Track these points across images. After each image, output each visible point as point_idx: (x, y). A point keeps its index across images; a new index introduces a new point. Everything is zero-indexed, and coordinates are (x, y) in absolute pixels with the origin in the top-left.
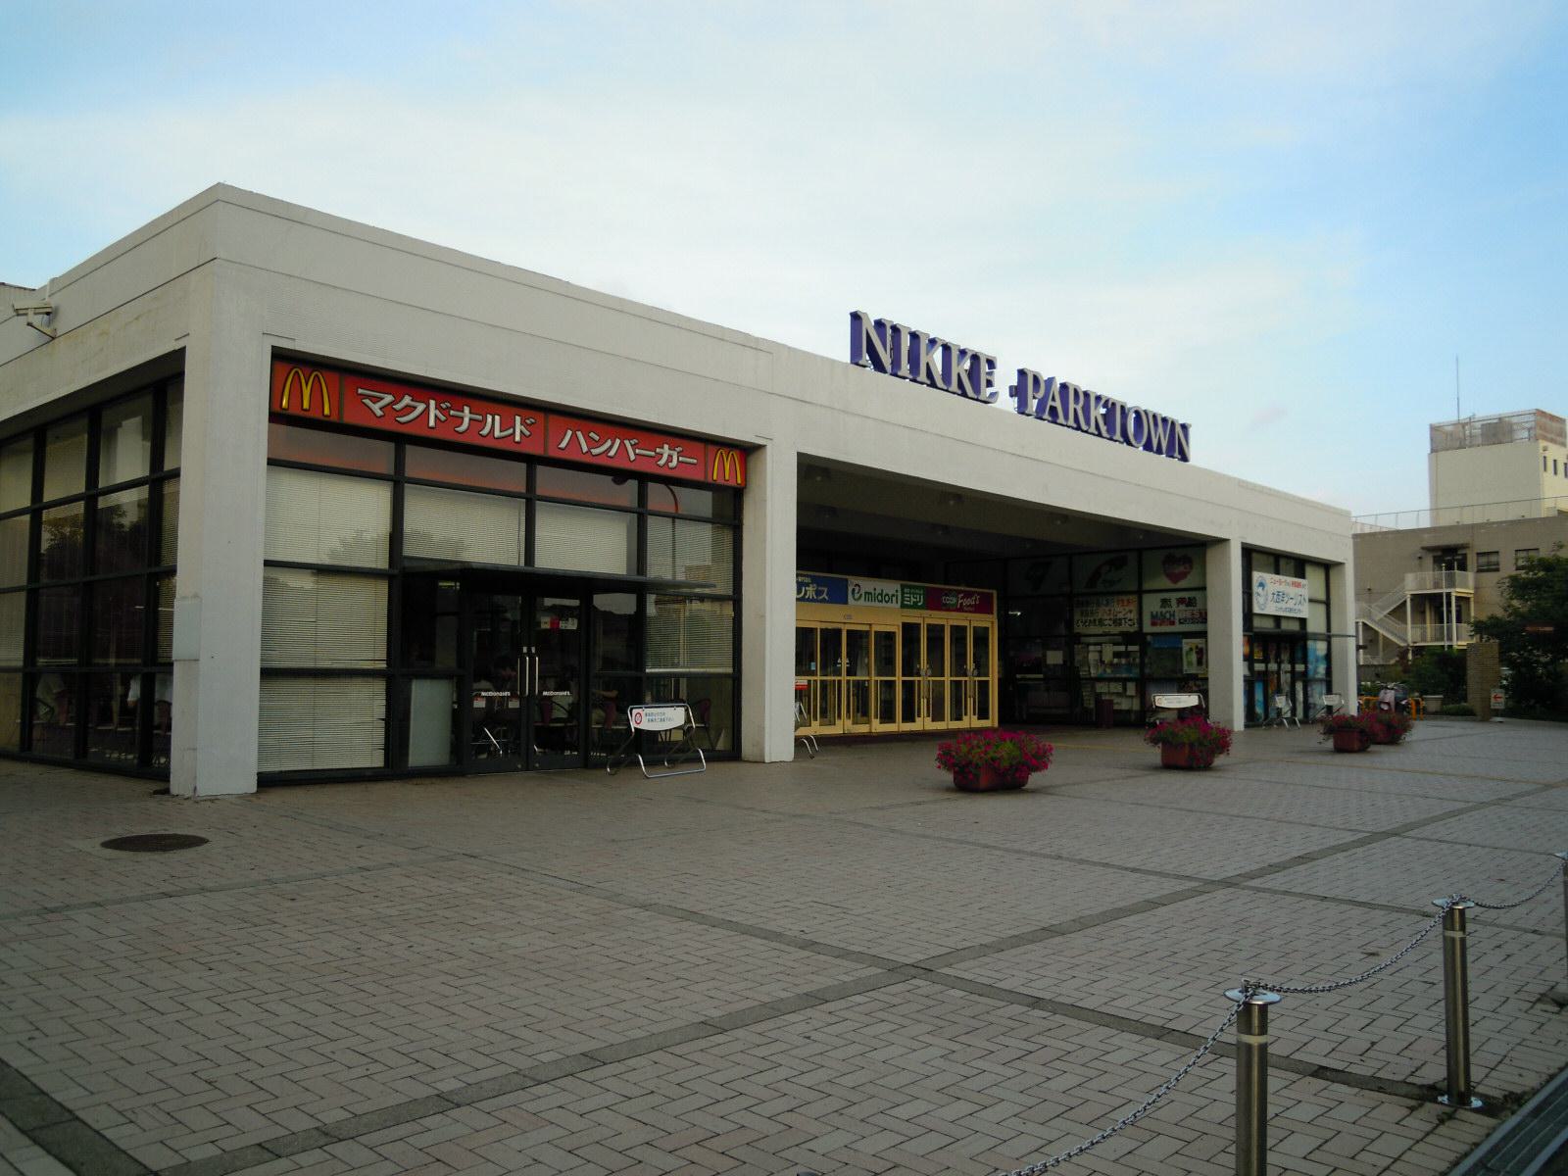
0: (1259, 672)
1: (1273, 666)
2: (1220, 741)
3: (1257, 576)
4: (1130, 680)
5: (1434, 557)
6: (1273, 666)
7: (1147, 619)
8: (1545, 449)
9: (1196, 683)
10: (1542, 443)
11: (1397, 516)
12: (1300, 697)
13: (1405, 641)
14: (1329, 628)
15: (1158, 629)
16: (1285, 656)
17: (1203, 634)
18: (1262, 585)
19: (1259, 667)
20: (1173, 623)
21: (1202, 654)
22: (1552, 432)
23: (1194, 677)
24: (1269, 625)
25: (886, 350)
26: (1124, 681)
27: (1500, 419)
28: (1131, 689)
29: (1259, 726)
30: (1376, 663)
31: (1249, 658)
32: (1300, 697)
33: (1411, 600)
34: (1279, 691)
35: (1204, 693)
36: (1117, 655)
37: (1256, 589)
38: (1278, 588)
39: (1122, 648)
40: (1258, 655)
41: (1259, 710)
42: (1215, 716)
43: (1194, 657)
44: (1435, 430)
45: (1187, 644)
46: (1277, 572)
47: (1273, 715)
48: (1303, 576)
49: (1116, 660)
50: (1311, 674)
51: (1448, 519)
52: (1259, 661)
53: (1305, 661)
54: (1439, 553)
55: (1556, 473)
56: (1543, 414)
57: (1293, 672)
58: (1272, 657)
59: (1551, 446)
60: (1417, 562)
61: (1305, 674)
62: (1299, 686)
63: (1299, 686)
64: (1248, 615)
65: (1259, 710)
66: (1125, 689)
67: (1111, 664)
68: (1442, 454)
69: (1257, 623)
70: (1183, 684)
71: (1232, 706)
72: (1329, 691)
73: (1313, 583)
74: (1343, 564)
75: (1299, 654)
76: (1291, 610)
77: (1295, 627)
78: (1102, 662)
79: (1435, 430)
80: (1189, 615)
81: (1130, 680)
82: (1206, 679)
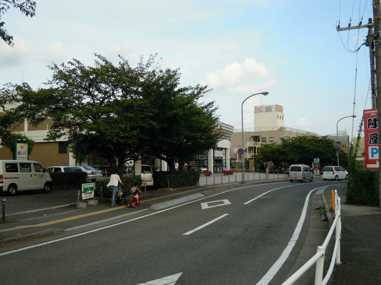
0: (215, 165)
1: (217, 164)
2: (211, 173)
3: (215, 151)
4: (197, 166)
5: (253, 138)
6: (217, 164)
7: (200, 158)
8: (278, 114)
9: (207, 167)
10: (277, 112)
11: (225, 154)
12: (221, 169)
13: (247, 157)
14: (226, 159)
15: (201, 159)
16: (219, 163)
17: (208, 160)
18: (216, 152)
19: (215, 164)
20: (203, 158)
21: (207, 163)
22: (280, 110)
23: (206, 166)
24: (217, 158)
25: (325, 274)
26: (196, 167)
27: (269, 106)
28: (197, 168)
29: (215, 173)
30: (241, 162)
31: (214, 163)
32: (221, 169)
33: (248, 148)
34: (218, 168)
35: (208, 168)
36: (195, 163)
37: (215, 153)
38: (218, 152)
39: (196, 162)
40: (215, 163)
41: (215, 171)
42: (209, 170)
43: (206, 163)
44: (255, 107)
45: (205, 161)
46: (218, 150)
47: (217, 171)
48: (222, 151)
49: (195, 164)
50: (223, 165)
51: (257, 130)
52: (215, 164)
53: (222, 163)
54: (254, 138)
55: (280, 119)
56: (278, 105)
57: (220, 165)
58: (217, 163)
59: (279, 113)
60: (250, 139)
61: (222, 165)
62: (221, 167)
63: (221, 167)
64: (214, 157)
65: (215, 171)
66: (196, 168)
67: (194, 164)
68: (257, 113)
69: (215, 158)
70: (205, 167)
71: (211, 169)
72: (226, 168)
73: (223, 151)
74: (228, 148)
75: (221, 162)
76: (220, 156)
77: (221, 158)
78: (193, 164)
79: (255, 107)
80: (206, 157)
81: (197, 166)
82: (208, 166)
